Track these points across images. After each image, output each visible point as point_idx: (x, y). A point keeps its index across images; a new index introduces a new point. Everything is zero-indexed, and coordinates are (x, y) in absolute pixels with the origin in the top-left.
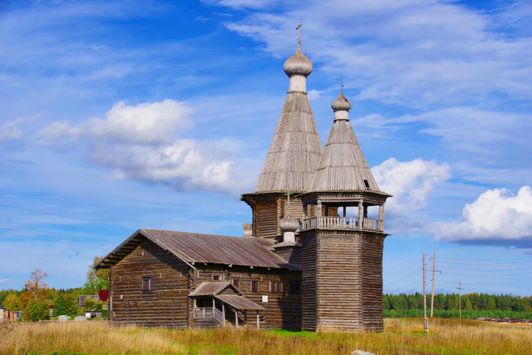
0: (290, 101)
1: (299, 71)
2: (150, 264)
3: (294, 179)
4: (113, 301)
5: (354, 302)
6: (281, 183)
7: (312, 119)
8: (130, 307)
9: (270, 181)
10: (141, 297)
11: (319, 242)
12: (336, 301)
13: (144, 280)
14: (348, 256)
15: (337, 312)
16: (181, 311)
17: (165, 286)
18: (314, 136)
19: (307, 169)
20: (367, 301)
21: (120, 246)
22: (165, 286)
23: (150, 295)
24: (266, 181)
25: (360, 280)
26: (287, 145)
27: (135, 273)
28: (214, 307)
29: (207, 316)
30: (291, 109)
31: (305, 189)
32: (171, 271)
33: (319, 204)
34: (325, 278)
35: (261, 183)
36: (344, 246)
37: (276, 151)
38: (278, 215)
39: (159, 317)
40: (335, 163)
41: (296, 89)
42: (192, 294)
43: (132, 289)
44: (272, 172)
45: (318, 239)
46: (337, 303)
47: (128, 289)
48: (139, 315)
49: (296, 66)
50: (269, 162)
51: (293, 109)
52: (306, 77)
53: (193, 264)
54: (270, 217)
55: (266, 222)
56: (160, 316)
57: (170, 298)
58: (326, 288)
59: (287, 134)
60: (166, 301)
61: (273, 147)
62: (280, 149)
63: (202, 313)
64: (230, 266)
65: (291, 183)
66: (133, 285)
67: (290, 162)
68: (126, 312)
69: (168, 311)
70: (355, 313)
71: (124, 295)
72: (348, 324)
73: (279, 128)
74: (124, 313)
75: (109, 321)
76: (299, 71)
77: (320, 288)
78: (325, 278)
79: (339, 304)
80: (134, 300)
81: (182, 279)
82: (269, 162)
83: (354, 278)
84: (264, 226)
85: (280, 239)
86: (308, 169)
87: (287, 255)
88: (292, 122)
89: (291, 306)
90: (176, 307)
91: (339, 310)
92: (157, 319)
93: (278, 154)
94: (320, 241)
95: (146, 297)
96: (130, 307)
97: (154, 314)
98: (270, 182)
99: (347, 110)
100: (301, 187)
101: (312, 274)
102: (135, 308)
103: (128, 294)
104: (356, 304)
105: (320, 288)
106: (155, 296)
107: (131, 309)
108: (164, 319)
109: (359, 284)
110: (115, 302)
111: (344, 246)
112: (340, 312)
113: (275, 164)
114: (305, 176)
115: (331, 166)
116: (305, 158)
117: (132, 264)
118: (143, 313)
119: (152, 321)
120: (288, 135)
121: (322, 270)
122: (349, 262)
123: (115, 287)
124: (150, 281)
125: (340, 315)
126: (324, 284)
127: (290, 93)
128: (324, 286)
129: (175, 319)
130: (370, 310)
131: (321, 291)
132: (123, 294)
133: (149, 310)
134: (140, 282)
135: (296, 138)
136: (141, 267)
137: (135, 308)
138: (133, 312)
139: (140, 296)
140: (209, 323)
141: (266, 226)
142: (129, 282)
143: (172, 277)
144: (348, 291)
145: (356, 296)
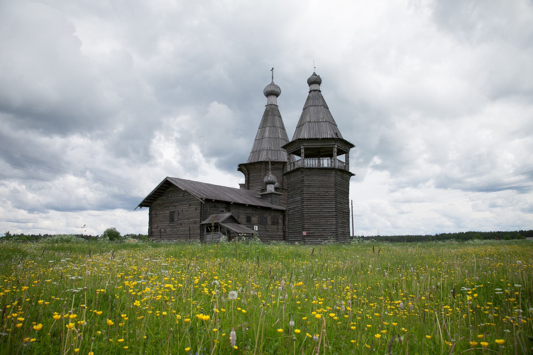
6: (263, 156)
9: (256, 156)
12: (318, 225)
14: (327, 189)
15: (319, 234)
20: (342, 225)
26: (267, 134)
34: (309, 206)
36: (323, 181)
37: (260, 138)
40: (313, 120)
46: (319, 226)
53: (204, 200)
58: (309, 215)
64: (232, 203)
70: (334, 234)
78: (309, 206)
79: (320, 227)
85: (264, 190)
89: (273, 233)
91: (320, 232)
93: (261, 140)
98: (257, 157)
104: (334, 227)
105: (305, 215)
109: (336, 211)
111: (323, 181)
115: (310, 122)
122: (327, 194)
125: (321, 236)
126: (307, 212)
130: (343, 232)
131: (305, 217)
133: (174, 235)
144: (327, 217)
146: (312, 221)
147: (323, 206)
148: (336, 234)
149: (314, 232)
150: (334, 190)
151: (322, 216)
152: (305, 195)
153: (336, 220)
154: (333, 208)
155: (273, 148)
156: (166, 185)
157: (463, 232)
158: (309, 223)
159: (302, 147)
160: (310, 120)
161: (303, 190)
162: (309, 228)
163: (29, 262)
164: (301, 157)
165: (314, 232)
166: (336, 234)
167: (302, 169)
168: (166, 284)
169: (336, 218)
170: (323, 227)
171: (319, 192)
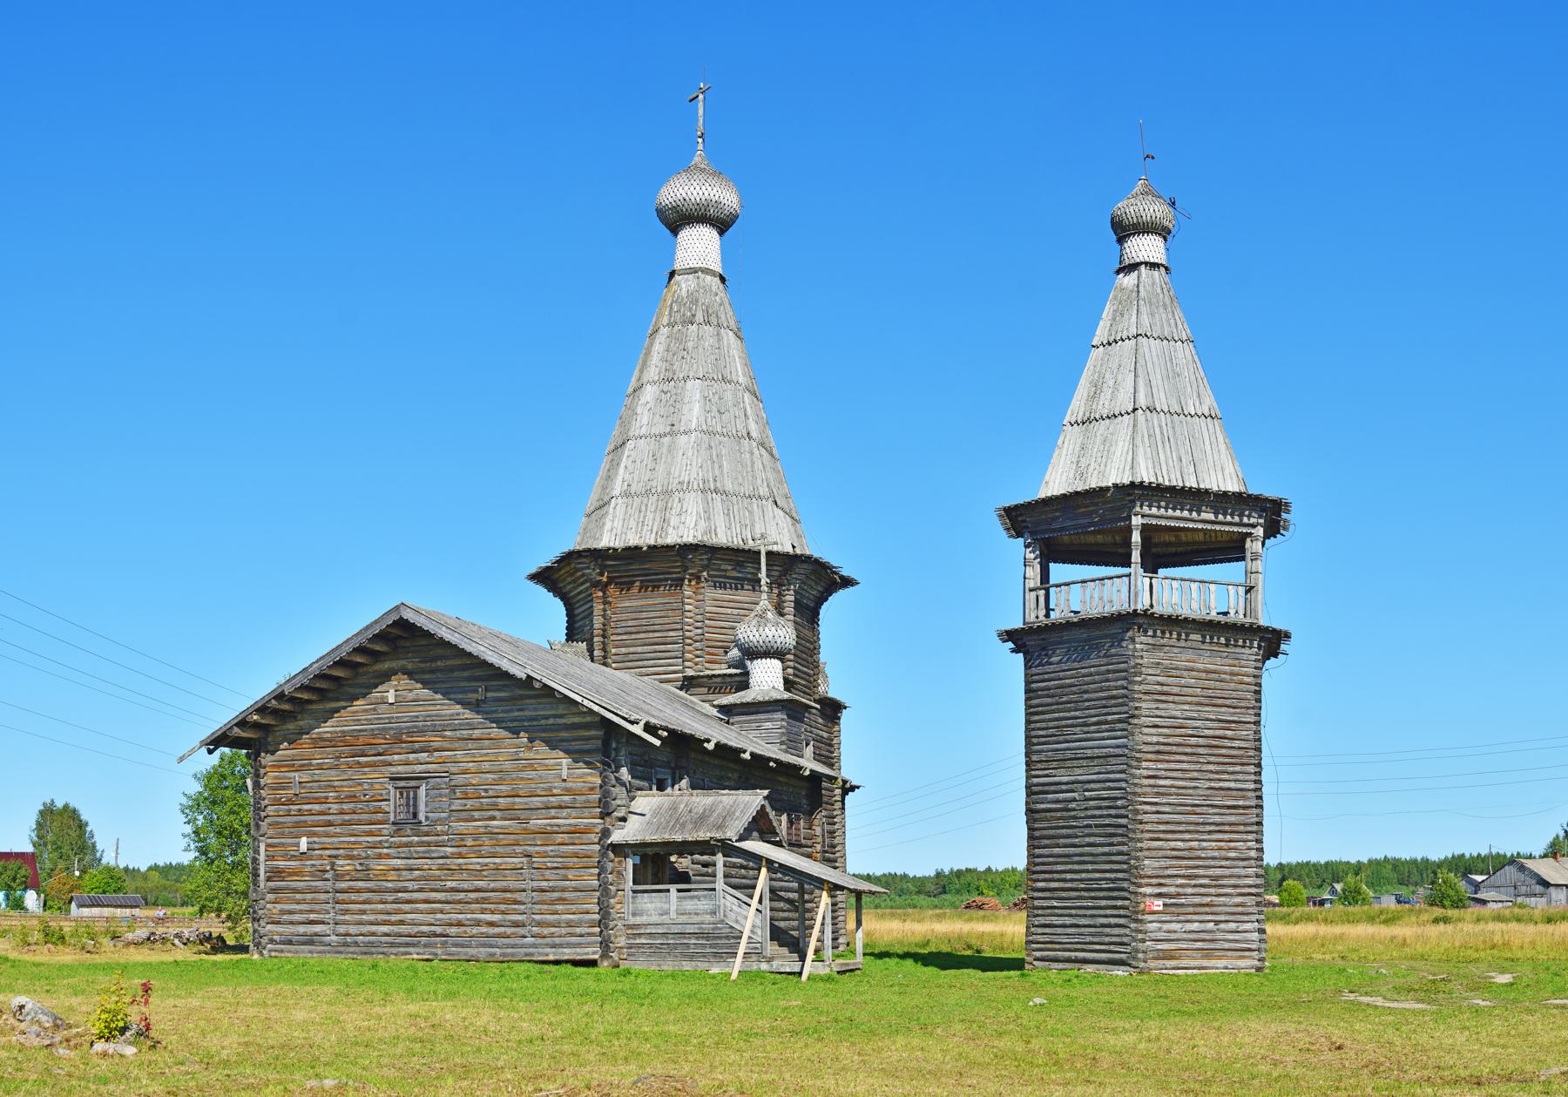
1: (712, 211)
2: (422, 731)
3: (726, 512)
4: (270, 858)
5: (1245, 863)
8: (338, 877)
9: (650, 516)
10: (386, 845)
11: (1140, 661)
13: (396, 788)
16: (566, 895)
19: (758, 489)
21: (315, 666)
22: (495, 807)
23: (426, 839)
24: (636, 516)
26: (693, 414)
27: (359, 763)
28: (720, 884)
29: (690, 914)
30: (694, 316)
32: (516, 757)
33: (1137, 529)
35: (616, 522)
38: (793, 598)
41: (700, 263)
42: (617, 836)
43: (347, 817)
44: (653, 491)
48: (381, 906)
49: (706, 194)
50: (638, 462)
52: (721, 233)
54: (656, 623)
55: (642, 635)
57: (518, 849)
59: (690, 384)
60: (497, 860)
61: (645, 421)
62: (669, 427)
63: (667, 906)
64: (710, 746)
66: (352, 805)
67: (709, 462)
68: (323, 896)
69: (508, 895)
71: (311, 840)
72: (1230, 937)
73: (658, 369)
74: (313, 899)
75: (256, 925)
76: (712, 211)
77: (1146, 818)
79: (1201, 872)
81: (569, 785)
82: (638, 462)
83: (1243, 786)
84: (632, 650)
86: (760, 488)
87: (771, 727)
90: (544, 884)
91: (1203, 890)
92: (460, 924)
93: (666, 440)
94: (1142, 657)
95: (407, 845)
96: (338, 877)
97: (447, 907)
99: (1163, 232)
101: (1097, 769)
103: (327, 835)
105: (1146, 818)
106: (449, 844)
107: (344, 885)
108: (491, 924)
110: (275, 863)
112: (1207, 900)
113: (661, 468)
114: (755, 506)
116: (748, 456)
118: (313, 902)
119: (439, 930)
120: (694, 389)
123: (275, 811)
124: (422, 792)
126: (1156, 804)
127: (681, 272)
128: (1158, 812)
129: (539, 924)
131: (1148, 827)
132: (309, 835)
133: (421, 890)
134: (381, 795)
135: (717, 397)
136: (384, 741)
138: (353, 897)
139: (380, 842)
140: (697, 938)
142: (331, 794)
146: (1173, 844)
147: (1213, 785)
148: (1259, 899)
149: (1180, 890)
155: (729, 486)
156: (394, 631)
158: (1161, 853)
159: (1136, 521)
160: (1150, 404)
162: (1160, 873)
163: (565, 988)
165: (1180, 890)
167: (1141, 621)
170: (1211, 872)
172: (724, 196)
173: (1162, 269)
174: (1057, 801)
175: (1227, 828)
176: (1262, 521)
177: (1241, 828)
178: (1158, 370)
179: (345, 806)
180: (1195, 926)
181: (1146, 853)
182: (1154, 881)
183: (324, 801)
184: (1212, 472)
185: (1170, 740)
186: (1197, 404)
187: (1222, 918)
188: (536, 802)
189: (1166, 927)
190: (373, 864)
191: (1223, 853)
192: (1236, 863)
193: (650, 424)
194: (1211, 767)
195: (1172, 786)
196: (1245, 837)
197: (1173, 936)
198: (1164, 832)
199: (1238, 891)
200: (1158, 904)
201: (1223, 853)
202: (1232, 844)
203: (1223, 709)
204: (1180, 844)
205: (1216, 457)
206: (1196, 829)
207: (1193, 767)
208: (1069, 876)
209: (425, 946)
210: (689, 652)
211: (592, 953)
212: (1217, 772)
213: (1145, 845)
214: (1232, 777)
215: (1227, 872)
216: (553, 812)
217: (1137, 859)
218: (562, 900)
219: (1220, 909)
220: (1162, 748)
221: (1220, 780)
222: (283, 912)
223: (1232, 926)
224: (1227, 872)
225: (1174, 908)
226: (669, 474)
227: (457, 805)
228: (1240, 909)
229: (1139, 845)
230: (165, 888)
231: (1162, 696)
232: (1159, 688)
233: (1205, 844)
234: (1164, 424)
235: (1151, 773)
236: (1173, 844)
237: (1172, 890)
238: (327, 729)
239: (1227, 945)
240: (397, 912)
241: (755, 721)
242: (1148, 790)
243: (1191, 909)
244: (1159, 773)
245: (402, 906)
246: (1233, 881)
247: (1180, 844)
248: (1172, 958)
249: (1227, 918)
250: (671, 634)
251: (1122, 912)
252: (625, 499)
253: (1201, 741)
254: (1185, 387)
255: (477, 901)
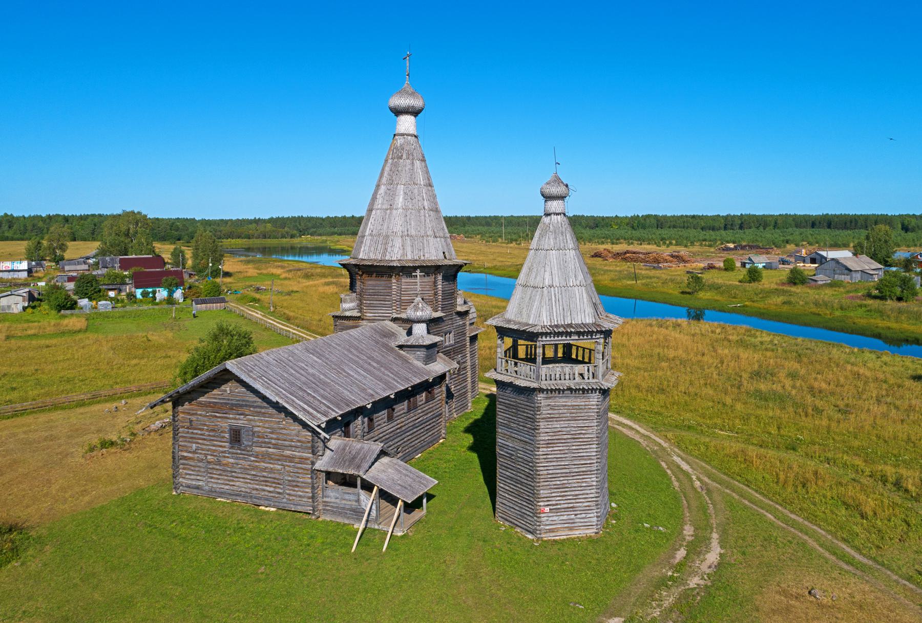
0: (399, 145)
2: (241, 406)
5: (590, 488)
6: (396, 250)
7: (426, 166)
11: (540, 405)
16: (299, 484)
17: (270, 443)
18: (430, 188)
25: (598, 457)
26: (400, 200)
30: (402, 156)
31: (426, 257)
34: (550, 456)
37: (384, 207)
39: (261, 487)
45: (537, 400)
47: (204, 437)
51: (404, 156)
56: (262, 485)
57: (280, 463)
61: (380, 202)
65: (409, 249)
72: (582, 520)
77: (541, 473)
78: (550, 456)
79: (568, 493)
80: (216, 456)
84: (372, 302)
88: (404, 172)
92: (257, 489)
97: (252, 482)
100: (422, 255)
102: (218, 467)
104: (593, 491)
105: (541, 473)
112: (572, 505)
114: (425, 240)
117: (209, 402)
120: (401, 188)
121: (544, 446)
122: (583, 432)
137: (218, 467)
141: (375, 302)
143: (281, 433)
145: (593, 479)
146: (554, 483)
147: (575, 455)
148: (597, 503)
150: (596, 424)
151: (573, 473)
152: (542, 435)
153: (597, 478)
154: (593, 458)
155: (413, 232)
157: (638, 216)
161: (539, 426)
164: (445, 218)
166: (597, 503)
168: (70, 244)
169: (597, 474)
171: (568, 429)
172: (416, 103)
173: (562, 215)
174: (507, 453)
175: (582, 473)
176: (602, 336)
177: (589, 473)
178: (555, 266)
179: (211, 434)
180: (565, 517)
181: (542, 488)
182: (545, 499)
183: (202, 430)
184: (579, 314)
185: (554, 438)
186: (574, 280)
187: (579, 512)
188: (287, 443)
189: (550, 519)
190: (221, 459)
191: (579, 485)
192: (586, 488)
193: (382, 204)
194: (574, 448)
195: (555, 458)
196: (590, 476)
197: (554, 523)
198: (550, 478)
199: (586, 500)
200: (547, 509)
201: (579, 485)
202: (584, 480)
203: (580, 422)
204: (558, 483)
205: (582, 305)
206: (566, 475)
207: (565, 448)
208: (512, 486)
209: (244, 497)
210: (395, 306)
211: (309, 509)
212: (577, 449)
213: (540, 484)
214: (585, 451)
215: (581, 492)
216: (293, 449)
217: (537, 490)
218: (297, 486)
219: (577, 509)
220: (550, 441)
221: (578, 453)
222: (187, 474)
223: (584, 516)
224: (581, 492)
225: (555, 511)
226: (388, 227)
227: (255, 439)
228: (588, 508)
229: (538, 484)
230: (274, 231)
231: (549, 419)
232: (549, 416)
233: (570, 481)
234: (557, 293)
235: (544, 453)
236: (554, 483)
237: (554, 502)
238: (201, 399)
239: (580, 524)
240: (233, 481)
241: (413, 351)
242: (543, 460)
243: (563, 510)
244: (548, 453)
245: (234, 479)
246: (584, 496)
247: (558, 483)
248: (553, 532)
249: (581, 512)
250: (387, 297)
251: (531, 510)
252: (370, 237)
253: (569, 436)
254: (569, 272)
255: (263, 481)
